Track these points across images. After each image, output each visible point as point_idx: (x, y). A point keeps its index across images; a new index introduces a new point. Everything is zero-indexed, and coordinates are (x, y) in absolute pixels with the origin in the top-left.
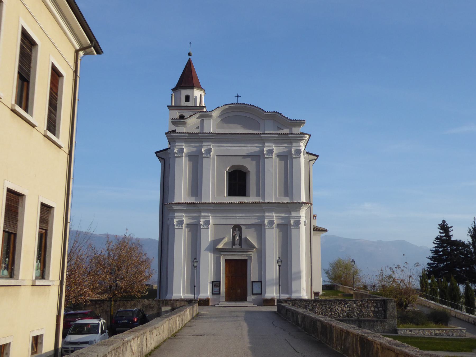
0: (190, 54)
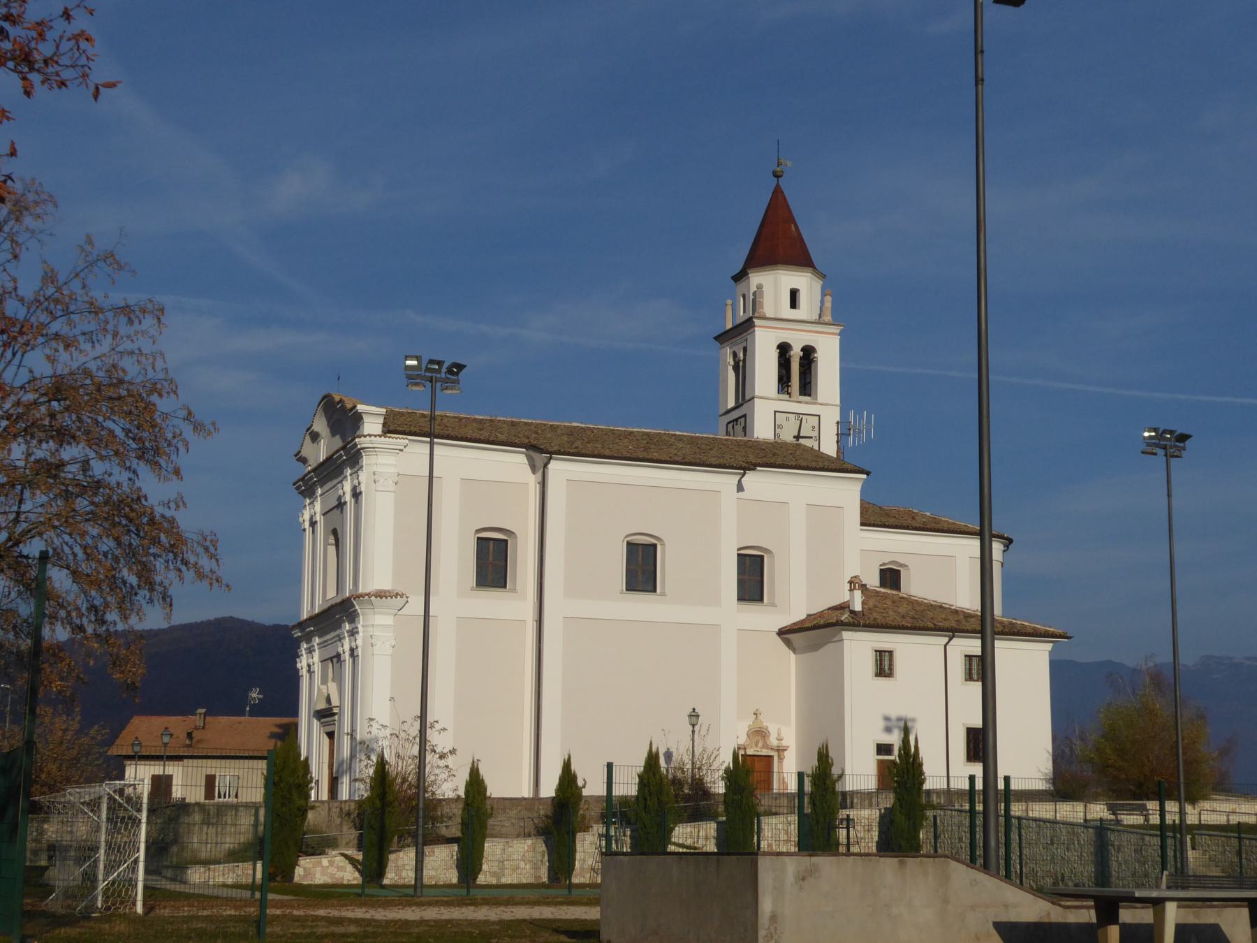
0: (777, 176)
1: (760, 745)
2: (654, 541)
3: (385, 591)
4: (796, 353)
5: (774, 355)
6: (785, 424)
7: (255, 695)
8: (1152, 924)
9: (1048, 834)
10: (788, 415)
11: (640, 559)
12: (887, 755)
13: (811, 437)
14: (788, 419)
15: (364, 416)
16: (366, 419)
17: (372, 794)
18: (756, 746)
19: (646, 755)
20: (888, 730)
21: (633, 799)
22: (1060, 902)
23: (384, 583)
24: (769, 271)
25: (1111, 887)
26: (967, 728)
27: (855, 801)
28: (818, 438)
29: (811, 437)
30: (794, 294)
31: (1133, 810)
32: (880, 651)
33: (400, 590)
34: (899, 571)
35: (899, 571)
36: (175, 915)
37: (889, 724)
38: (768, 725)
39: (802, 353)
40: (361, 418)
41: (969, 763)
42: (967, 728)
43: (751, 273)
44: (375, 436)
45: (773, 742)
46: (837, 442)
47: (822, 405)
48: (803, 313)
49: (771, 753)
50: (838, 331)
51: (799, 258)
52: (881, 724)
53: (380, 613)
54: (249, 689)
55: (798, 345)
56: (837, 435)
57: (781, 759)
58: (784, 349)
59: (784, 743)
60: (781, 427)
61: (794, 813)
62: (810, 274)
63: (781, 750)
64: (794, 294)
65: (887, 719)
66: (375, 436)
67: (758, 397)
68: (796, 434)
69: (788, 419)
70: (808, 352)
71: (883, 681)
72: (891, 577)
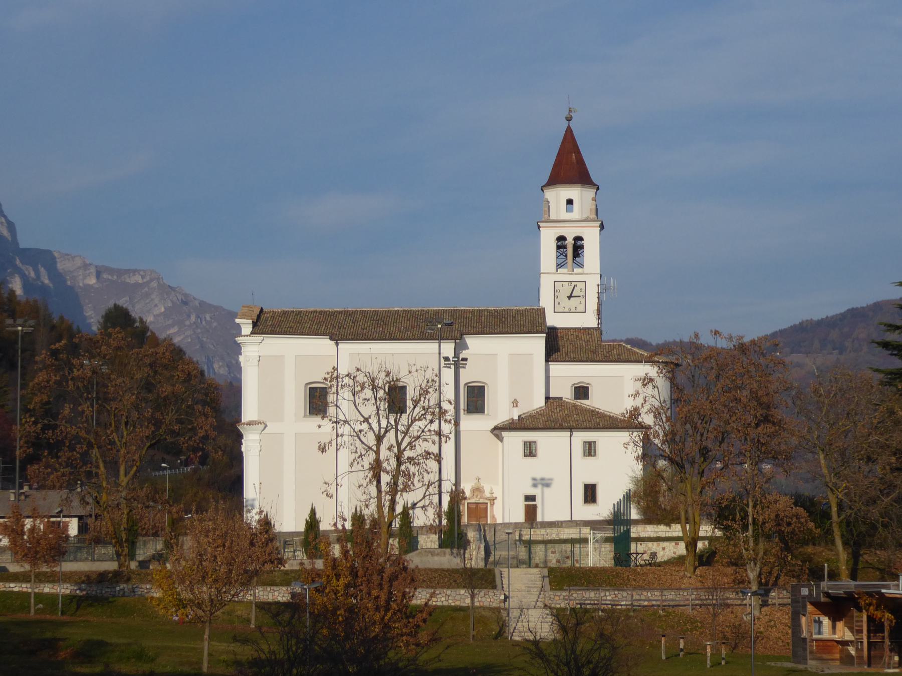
1: (479, 497)
2: (405, 384)
3: (253, 421)
4: (570, 242)
5: (553, 245)
6: (561, 289)
11: (641, 352)
13: (580, 296)
14: (563, 286)
15: (241, 325)
16: (242, 326)
17: (9, 536)
18: (477, 497)
19: (310, 509)
20: (535, 486)
21: (704, 523)
23: (254, 418)
25: (842, 581)
26: (585, 485)
27: (486, 528)
29: (580, 296)
30: (570, 202)
31: (608, 531)
32: (530, 443)
33: (261, 419)
34: (588, 387)
35: (588, 387)
36: (109, 590)
37: (535, 482)
38: (484, 485)
40: (240, 326)
41: (586, 505)
42: (585, 485)
44: (247, 336)
45: (487, 494)
46: (598, 297)
47: (587, 274)
48: (575, 214)
49: (486, 501)
50: (599, 225)
51: (582, 177)
52: (530, 482)
53: (251, 433)
55: (570, 234)
56: (598, 293)
57: (492, 505)
58: (561, 239)
59: (494, 495)
60: (558, 291)
62: (579, 188)
63: (493, 500)
64: (570, 202)
65: (534, 479)
66: (247, 336)
67: (543, 273)
68: (569, 295)
69: (563, 286)
70: (578, 239)
71: (530, 460)
72: (582, 392)
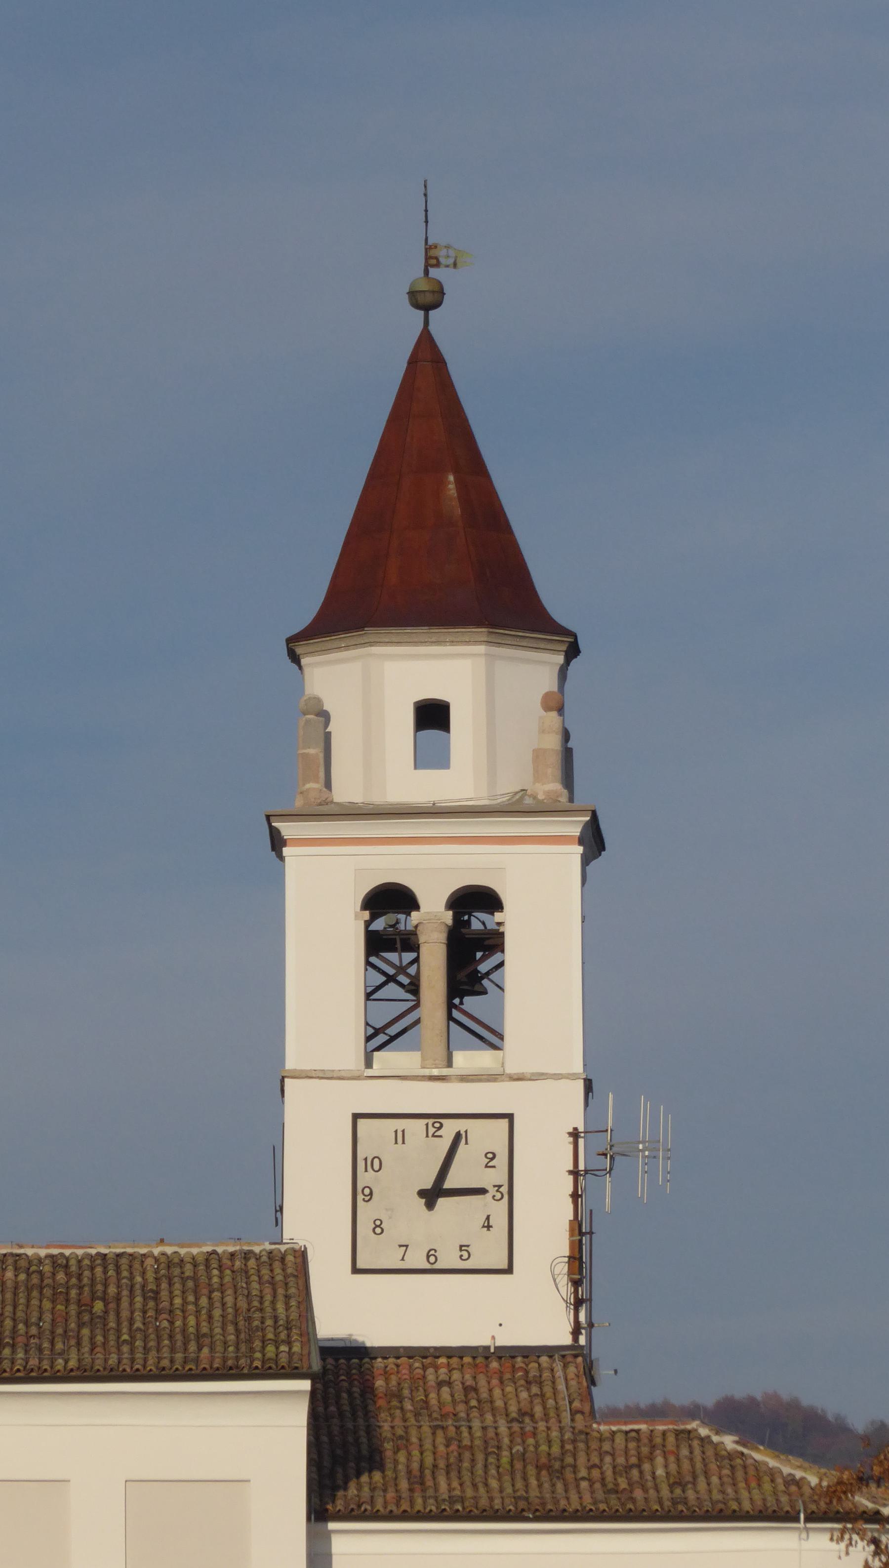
6: (389, 1153)
7: (479, 975)
8: (411, 982)
9: (660, 1472)
10: (365, 1228)
12: (396, 941)
13: (482, 1191)
14: (400, 1137)
22: (416, 1002)
24: (347, 648)
28: (505, 1189)
29: (482, 1191)
39: (451, 913)
43: (311, 653)
46: (575, 1196)
54: (478, 975)
56: (575, 1173)
61: (423, 1067)
62: (481, 649)
68: (428, 1184)
